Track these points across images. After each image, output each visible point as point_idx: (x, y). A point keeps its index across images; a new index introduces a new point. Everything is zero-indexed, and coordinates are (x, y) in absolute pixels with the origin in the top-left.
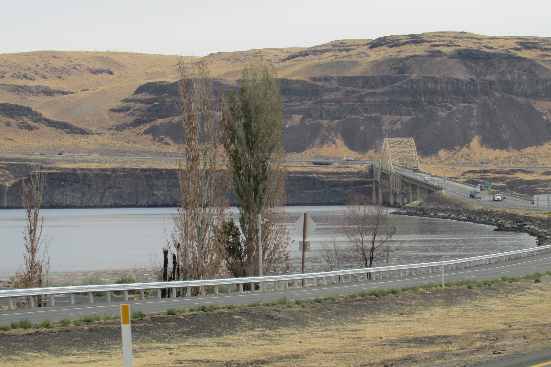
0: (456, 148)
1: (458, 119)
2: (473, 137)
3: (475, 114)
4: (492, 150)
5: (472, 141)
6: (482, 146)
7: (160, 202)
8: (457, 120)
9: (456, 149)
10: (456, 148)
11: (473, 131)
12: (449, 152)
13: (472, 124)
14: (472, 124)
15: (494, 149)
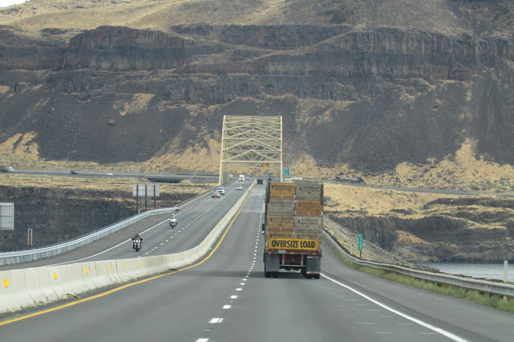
0: (429, 160)
1: (436, 107)
2: (462, 141)
3: (469, 99)
4: (496, 165)
5: (460, 147)
6: (478, 158)
7: (487, 258)
8: (436, 110)
9: (429, 163)
10: (429, 160)
11: (464, 131)
12: (415, 167)
13: (462, 116)
14: (462, 116)
15: (501, 164)
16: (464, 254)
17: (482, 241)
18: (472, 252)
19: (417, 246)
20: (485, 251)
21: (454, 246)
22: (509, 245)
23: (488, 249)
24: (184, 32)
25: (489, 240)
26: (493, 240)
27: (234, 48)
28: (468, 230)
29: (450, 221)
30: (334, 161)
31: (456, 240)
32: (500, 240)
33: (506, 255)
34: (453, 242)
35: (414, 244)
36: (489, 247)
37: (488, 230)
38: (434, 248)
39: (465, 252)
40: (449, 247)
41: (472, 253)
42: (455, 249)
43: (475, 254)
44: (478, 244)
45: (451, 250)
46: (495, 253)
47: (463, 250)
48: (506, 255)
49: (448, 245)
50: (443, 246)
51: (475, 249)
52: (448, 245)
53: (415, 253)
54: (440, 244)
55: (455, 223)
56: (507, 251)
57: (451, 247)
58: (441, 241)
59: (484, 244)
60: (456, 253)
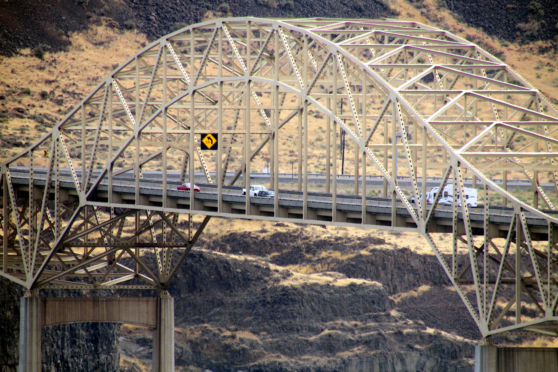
16: (283, 359)
17: (324, 320)
18: (303, 352)
19: (139, 336)
20: (340, 350)
21: (245, 335)
22: (405, 331)
23: (349, 344)
24: (503, 339)
25: (343, 316)
26: (355, 319)
27: (57, 237)
28: (284, 289)
29: (227, 265)
30: (97, 324)
31: (249, 318)
32: (376, 319)
33: (402, 360)
34: (242, 326)
35: (130, 332)
36: (350, 336)
37: (336, 291)
38: (190, 341)
39: (285, 354)
40: (237, 340)
41: (306, 357)
42: (253, 345)
43: (315, 359)
44: (317, 331)
45: (243, 349)
46: (375, 355)
47: (278, 348)
48: (402, 360)
49: (228, 333)
50: (214, 335)
51: (311, 344)
52: (228, 333)
53: (139, 358)
54: (205, 332)
55: (239, 270)
56: (401, 348)
57: (241, 340)
58: (203, 322)
59: (334, 328)
60: (260, 356)
